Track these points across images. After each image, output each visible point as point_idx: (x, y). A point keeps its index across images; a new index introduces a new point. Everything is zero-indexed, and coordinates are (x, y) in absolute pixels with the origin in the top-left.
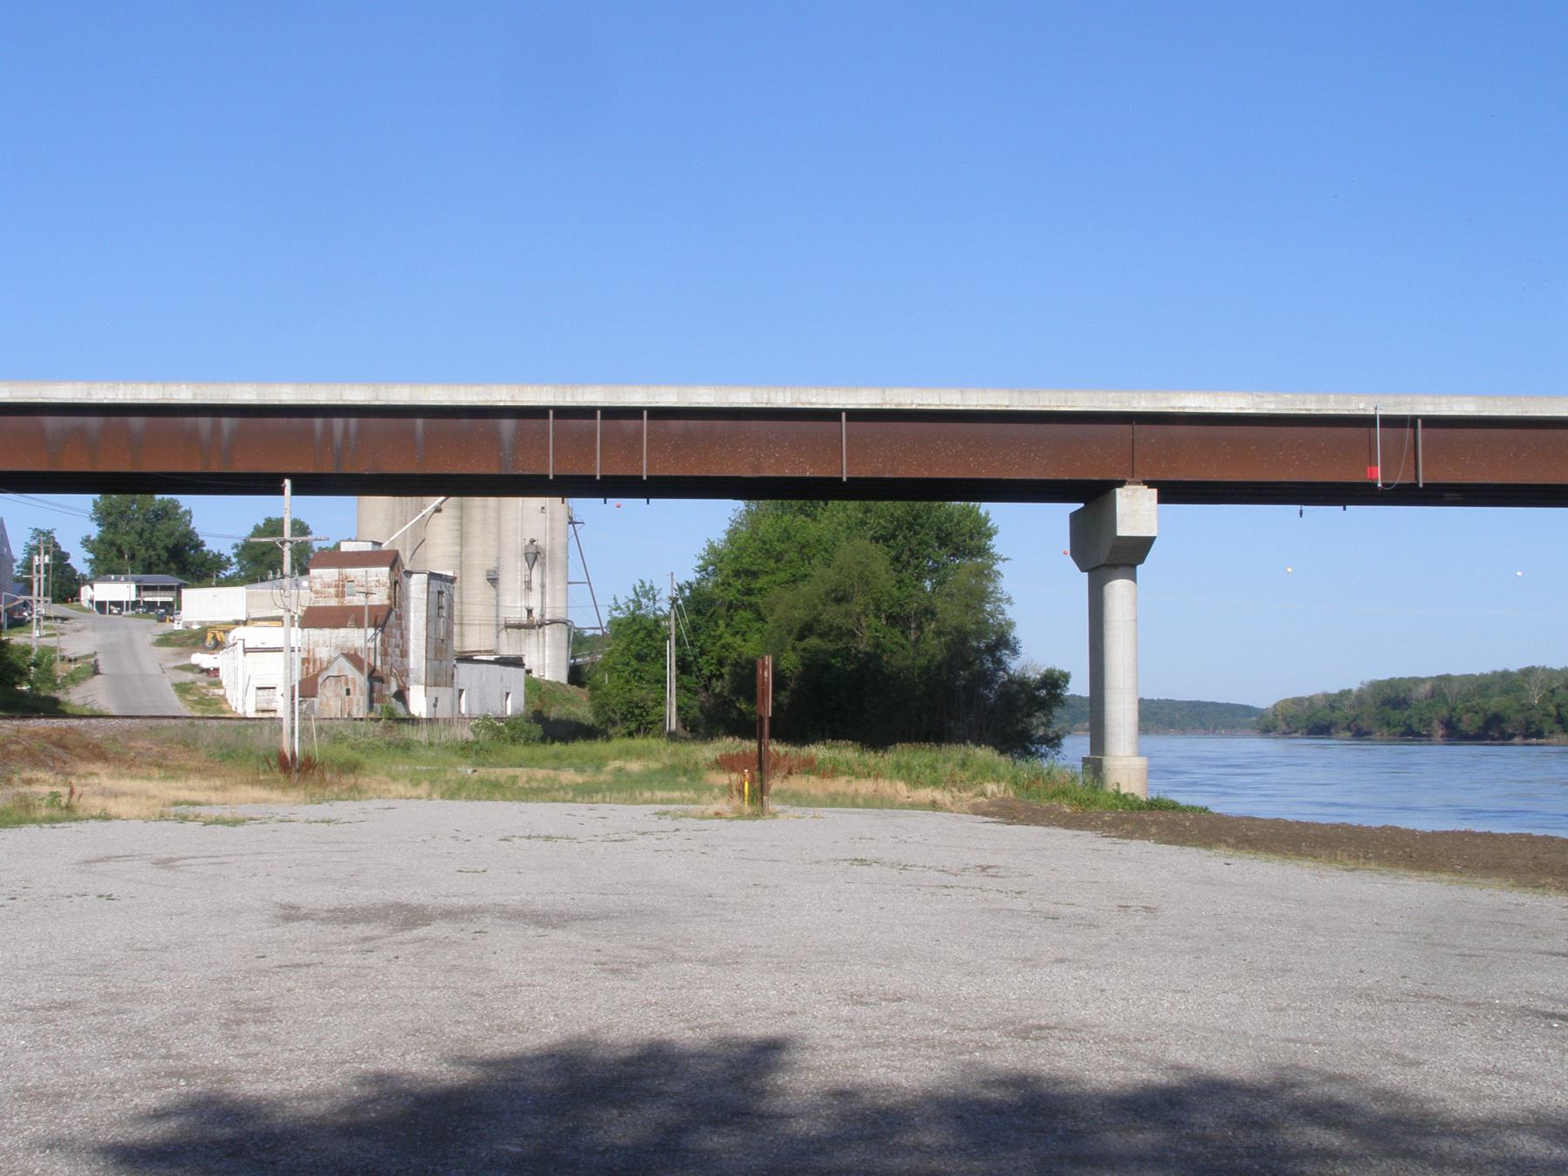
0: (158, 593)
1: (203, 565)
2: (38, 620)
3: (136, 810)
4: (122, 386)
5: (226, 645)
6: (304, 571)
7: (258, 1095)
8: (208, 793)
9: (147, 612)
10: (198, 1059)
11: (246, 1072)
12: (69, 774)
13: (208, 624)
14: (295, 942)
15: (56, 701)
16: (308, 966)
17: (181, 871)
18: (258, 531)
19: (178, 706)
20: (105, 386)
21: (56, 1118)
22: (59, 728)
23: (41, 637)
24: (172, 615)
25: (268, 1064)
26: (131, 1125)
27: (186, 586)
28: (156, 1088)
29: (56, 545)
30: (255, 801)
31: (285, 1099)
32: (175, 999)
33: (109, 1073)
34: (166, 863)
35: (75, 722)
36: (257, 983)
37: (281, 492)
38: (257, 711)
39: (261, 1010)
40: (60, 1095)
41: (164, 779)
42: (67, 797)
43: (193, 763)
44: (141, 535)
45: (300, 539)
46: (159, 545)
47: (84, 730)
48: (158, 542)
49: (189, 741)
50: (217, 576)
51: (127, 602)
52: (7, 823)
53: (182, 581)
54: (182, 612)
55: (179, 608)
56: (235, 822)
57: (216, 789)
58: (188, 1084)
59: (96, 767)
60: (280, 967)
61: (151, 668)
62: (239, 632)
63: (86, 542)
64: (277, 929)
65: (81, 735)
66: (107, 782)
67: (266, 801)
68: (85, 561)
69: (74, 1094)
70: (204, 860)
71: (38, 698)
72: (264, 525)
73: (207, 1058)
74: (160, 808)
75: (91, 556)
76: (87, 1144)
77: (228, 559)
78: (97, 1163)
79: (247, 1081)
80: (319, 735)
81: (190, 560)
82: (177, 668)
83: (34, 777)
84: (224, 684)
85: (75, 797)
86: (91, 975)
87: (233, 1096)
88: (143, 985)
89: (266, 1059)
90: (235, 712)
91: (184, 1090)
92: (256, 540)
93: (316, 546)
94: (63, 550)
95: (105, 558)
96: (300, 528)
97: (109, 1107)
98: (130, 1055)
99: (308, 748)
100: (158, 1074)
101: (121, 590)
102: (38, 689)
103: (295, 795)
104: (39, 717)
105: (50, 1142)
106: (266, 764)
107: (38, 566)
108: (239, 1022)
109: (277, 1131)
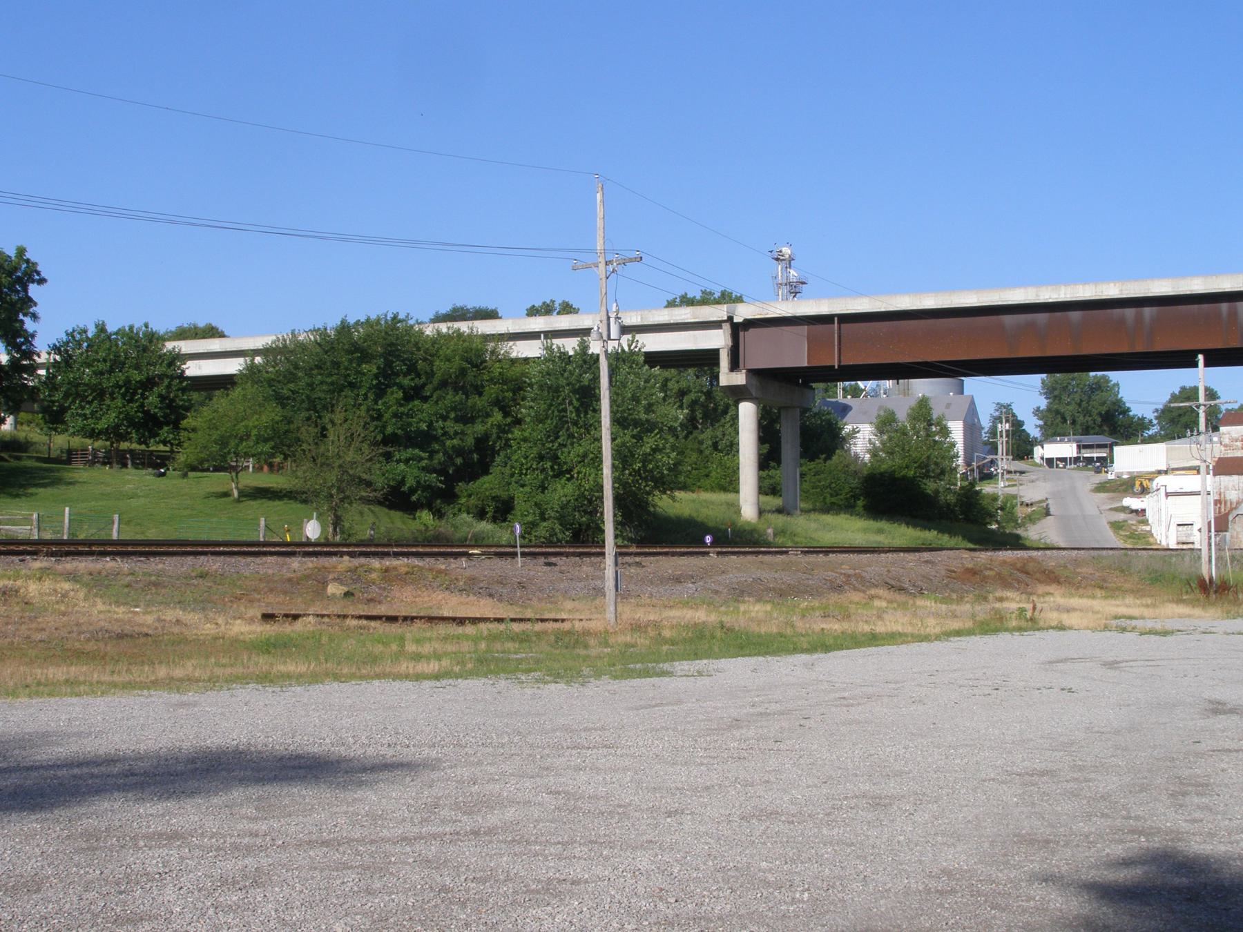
0: (1095, 450)
1: (1130, 426)
2: (1003, 474)
3: (1085, 622)
4: (1063, 287)
5: (1151, 491)
6: (1216, 429)
7: (1207, 853)
8: (1142, 609)
9: (1086, 466)
10: (1153, 821)
11: (1194, 834)
12: (1031, 594)
13: (1135, 474)
14: (1223, 731)
15: (1018, 537)
16: (1237, 751)
17: (1124, 671)
18: (1174, 398)
19: (1113, 539)
20: (1050, 288)
21: (1047, 859)
22: (1022, 558)
23: (1005, 487)
24: (1106, 467)
25: (1211, 829)
26: (1105, 869)
27: (1117, 444)
28: (1121, 841)
29: (1014, 415)
30: (1180, 616)
31: (1230, 858)
32: (1129, 773)
33: (1082, 827)
34: (1112, 665)
35: (1034, 553)
36: (1196, 763)
37: (1195, 365)
38: (1178, 543)
39: (1202, 785)
40: (1047, 842)
41: (1106, 598)
42: (1031, 611)
43: (1127, 586)
44: (1080, 405)
45: (1212, 403)
46: (1095, 412)
47: (1041, 559)
48: (1094, 410)
49: (1124, 567)
50: (1142, 435)
51: (1070, 458)
52: (987, 631)
53: (1114, 440)
54: (1114, 465)
55: (1112, 462)
56: (1165, 633)
57: (1147, 606)
58: (1147, 841)
59: (1051, 588)
60: (1214, 751)
61: (1091, 510)
62: (1161, 480)
63: (1037, 412)
64: (1207, 720)
65: (1039, 563)
66: (1061, 600)
67: (1189, 616)
68: (1037, 426)
69: (1058, 842)
70: (1142, 662)
71: (1004, 534)
72: (1180, 392)
73: (1160, 821)
74: (1104, 621)
75: (1041, 423)
76: (1073, 880)
77: (1151, 421)
78: (1083, 897)
79: (1196, 842)
80: (1232, 562)
81: (1120, 423)
82: (1111, 509)
83: (1004, 596)
84: (1150, 522)
85: (1036, 613)
86: (1061, 751)
87: (1185, 853)
88: (1103, 761)
89: (1209, 825)
90: (1160, 544)
91: (1145, 845)
92: (1176, 405)
93: (1223, 408)
94: (1019, 419)
95: (1052, 424)
96: (1211, 394)
97: (1087, 854)
98: (1099, 814)
99: (1223, 573)
100: (1122, 830)
101: (1065, 449)
102: (1004, 528)
103: (1212, 612)
104: (1007, 550)
105: (1045, 877)
106: (1188, 586)
107: (1001, 432)
108: (1185, 794)
109: (1226, 884)
